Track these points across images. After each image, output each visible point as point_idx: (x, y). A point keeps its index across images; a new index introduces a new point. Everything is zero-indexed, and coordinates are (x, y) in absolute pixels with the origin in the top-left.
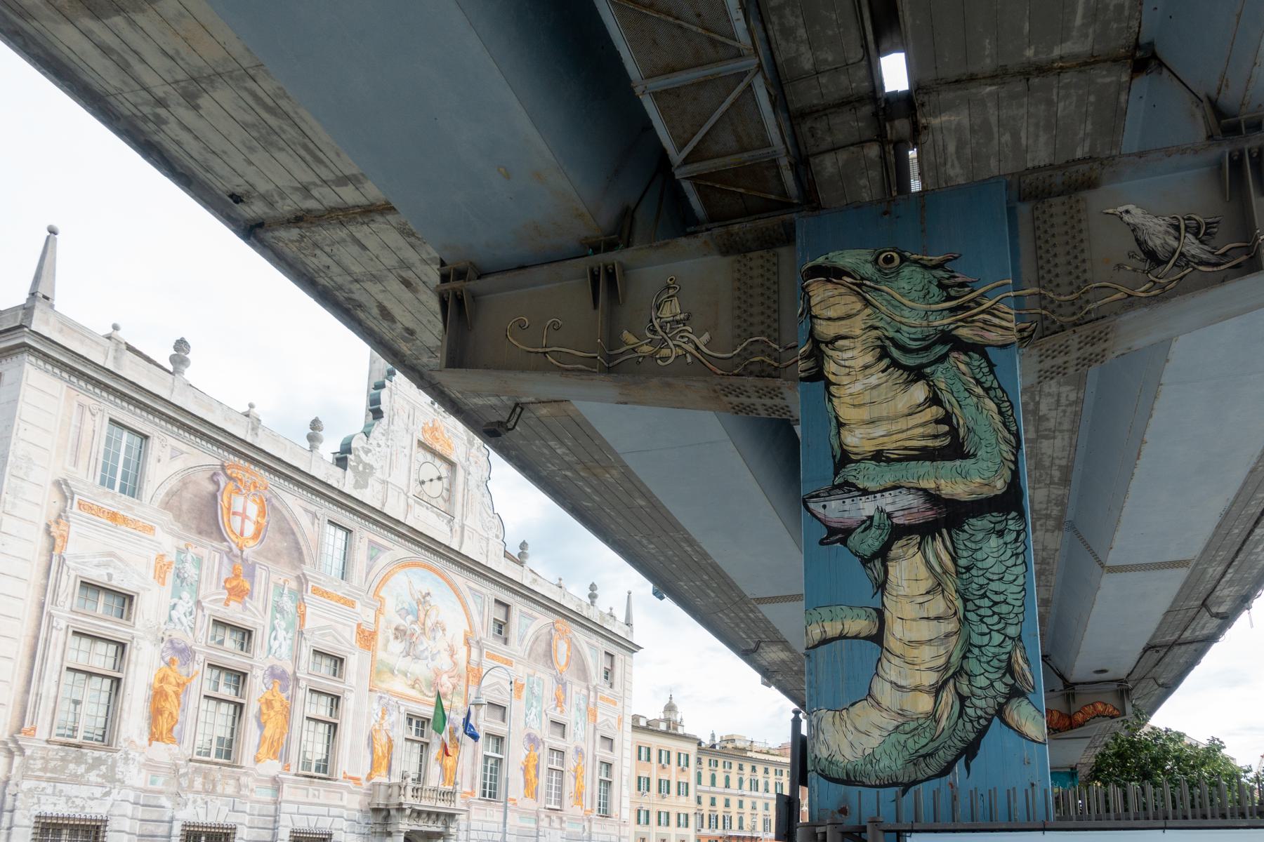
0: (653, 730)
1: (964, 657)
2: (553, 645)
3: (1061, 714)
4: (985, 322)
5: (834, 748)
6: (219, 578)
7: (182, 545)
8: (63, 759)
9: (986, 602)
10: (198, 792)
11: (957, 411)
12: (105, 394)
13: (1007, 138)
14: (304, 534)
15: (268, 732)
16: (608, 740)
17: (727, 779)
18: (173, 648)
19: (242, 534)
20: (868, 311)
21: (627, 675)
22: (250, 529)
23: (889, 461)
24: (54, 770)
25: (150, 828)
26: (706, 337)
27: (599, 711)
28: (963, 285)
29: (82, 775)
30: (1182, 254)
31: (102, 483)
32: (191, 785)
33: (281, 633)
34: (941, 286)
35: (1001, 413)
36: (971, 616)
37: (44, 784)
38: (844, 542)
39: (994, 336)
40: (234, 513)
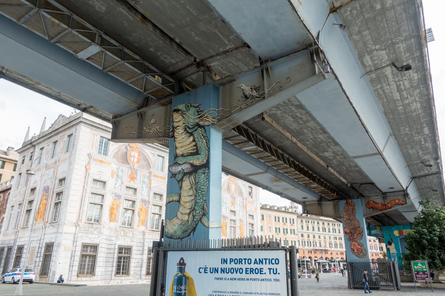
0: (279, 211)
1: (195, 206)
2: (230, 185)
3: (382, 204)
4: (205, 120)
5: (169, 229)
6: (127, 175)
7: (118, 167)
8: (88, 227)
9: (200, 191)
10: (122, 236)
11: (198, 143)
12: (99, 130)
13: (231, 64)
14: (150, 160)
15: (141, 218)
16: (252, 216)
17: (313, 227)
18: (116, 195)
19: (134, 162)
20: (183, 119)
21: (257, 194)
22: (136, 160)
23: (185, 156)
24: (86, 231)
25: (110, 246)
26: (159, 127)
27: (248, 206)
28: (202, 111)
29: (93, 232)
30: (252, 96)
31: (99, 153)
32: (120, 234)
33: (145, 189)
34: (198, 112)
35: (206, 143)
36: (197, 195)
37: (84, 234)
38: (175, 177)
39: (206, 123)
40: (132, 156)
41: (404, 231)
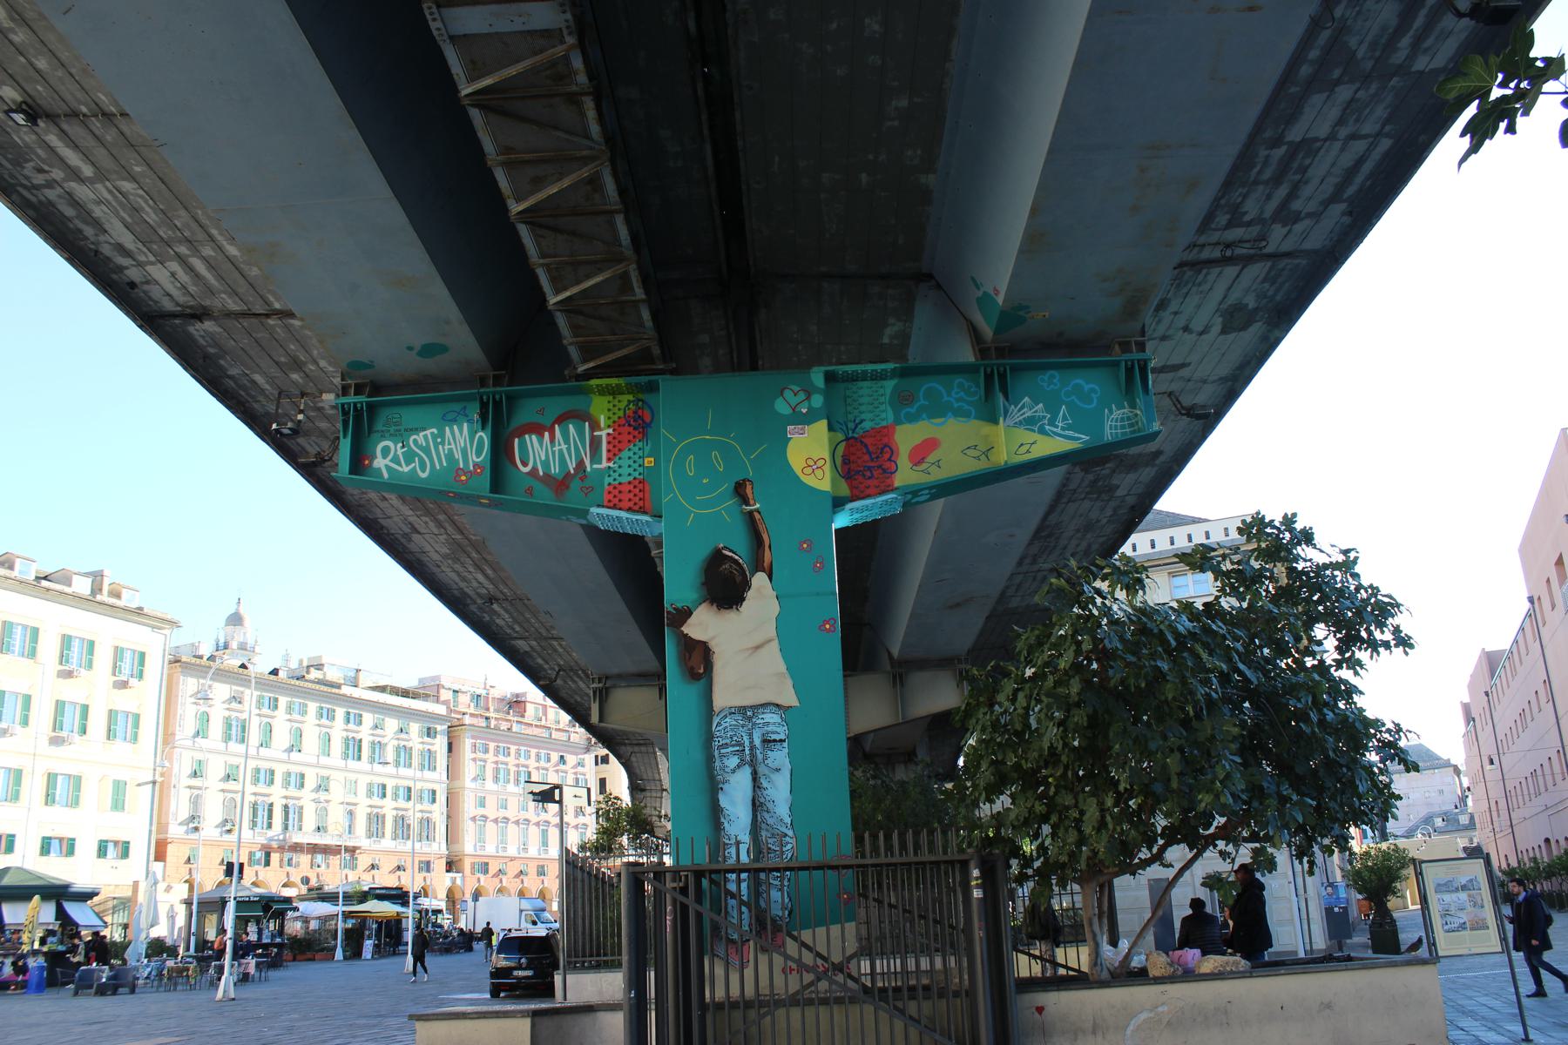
41: (907, 437)
